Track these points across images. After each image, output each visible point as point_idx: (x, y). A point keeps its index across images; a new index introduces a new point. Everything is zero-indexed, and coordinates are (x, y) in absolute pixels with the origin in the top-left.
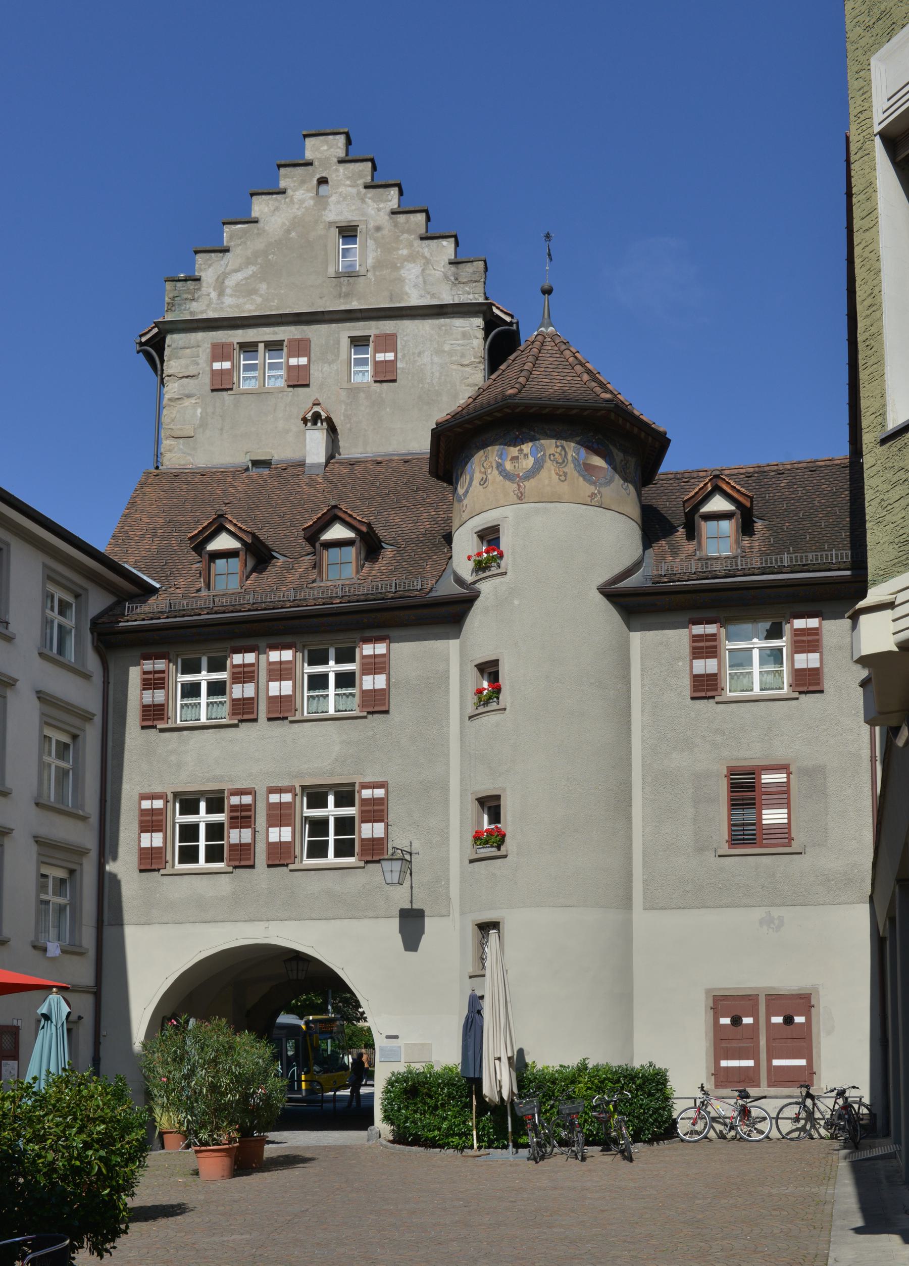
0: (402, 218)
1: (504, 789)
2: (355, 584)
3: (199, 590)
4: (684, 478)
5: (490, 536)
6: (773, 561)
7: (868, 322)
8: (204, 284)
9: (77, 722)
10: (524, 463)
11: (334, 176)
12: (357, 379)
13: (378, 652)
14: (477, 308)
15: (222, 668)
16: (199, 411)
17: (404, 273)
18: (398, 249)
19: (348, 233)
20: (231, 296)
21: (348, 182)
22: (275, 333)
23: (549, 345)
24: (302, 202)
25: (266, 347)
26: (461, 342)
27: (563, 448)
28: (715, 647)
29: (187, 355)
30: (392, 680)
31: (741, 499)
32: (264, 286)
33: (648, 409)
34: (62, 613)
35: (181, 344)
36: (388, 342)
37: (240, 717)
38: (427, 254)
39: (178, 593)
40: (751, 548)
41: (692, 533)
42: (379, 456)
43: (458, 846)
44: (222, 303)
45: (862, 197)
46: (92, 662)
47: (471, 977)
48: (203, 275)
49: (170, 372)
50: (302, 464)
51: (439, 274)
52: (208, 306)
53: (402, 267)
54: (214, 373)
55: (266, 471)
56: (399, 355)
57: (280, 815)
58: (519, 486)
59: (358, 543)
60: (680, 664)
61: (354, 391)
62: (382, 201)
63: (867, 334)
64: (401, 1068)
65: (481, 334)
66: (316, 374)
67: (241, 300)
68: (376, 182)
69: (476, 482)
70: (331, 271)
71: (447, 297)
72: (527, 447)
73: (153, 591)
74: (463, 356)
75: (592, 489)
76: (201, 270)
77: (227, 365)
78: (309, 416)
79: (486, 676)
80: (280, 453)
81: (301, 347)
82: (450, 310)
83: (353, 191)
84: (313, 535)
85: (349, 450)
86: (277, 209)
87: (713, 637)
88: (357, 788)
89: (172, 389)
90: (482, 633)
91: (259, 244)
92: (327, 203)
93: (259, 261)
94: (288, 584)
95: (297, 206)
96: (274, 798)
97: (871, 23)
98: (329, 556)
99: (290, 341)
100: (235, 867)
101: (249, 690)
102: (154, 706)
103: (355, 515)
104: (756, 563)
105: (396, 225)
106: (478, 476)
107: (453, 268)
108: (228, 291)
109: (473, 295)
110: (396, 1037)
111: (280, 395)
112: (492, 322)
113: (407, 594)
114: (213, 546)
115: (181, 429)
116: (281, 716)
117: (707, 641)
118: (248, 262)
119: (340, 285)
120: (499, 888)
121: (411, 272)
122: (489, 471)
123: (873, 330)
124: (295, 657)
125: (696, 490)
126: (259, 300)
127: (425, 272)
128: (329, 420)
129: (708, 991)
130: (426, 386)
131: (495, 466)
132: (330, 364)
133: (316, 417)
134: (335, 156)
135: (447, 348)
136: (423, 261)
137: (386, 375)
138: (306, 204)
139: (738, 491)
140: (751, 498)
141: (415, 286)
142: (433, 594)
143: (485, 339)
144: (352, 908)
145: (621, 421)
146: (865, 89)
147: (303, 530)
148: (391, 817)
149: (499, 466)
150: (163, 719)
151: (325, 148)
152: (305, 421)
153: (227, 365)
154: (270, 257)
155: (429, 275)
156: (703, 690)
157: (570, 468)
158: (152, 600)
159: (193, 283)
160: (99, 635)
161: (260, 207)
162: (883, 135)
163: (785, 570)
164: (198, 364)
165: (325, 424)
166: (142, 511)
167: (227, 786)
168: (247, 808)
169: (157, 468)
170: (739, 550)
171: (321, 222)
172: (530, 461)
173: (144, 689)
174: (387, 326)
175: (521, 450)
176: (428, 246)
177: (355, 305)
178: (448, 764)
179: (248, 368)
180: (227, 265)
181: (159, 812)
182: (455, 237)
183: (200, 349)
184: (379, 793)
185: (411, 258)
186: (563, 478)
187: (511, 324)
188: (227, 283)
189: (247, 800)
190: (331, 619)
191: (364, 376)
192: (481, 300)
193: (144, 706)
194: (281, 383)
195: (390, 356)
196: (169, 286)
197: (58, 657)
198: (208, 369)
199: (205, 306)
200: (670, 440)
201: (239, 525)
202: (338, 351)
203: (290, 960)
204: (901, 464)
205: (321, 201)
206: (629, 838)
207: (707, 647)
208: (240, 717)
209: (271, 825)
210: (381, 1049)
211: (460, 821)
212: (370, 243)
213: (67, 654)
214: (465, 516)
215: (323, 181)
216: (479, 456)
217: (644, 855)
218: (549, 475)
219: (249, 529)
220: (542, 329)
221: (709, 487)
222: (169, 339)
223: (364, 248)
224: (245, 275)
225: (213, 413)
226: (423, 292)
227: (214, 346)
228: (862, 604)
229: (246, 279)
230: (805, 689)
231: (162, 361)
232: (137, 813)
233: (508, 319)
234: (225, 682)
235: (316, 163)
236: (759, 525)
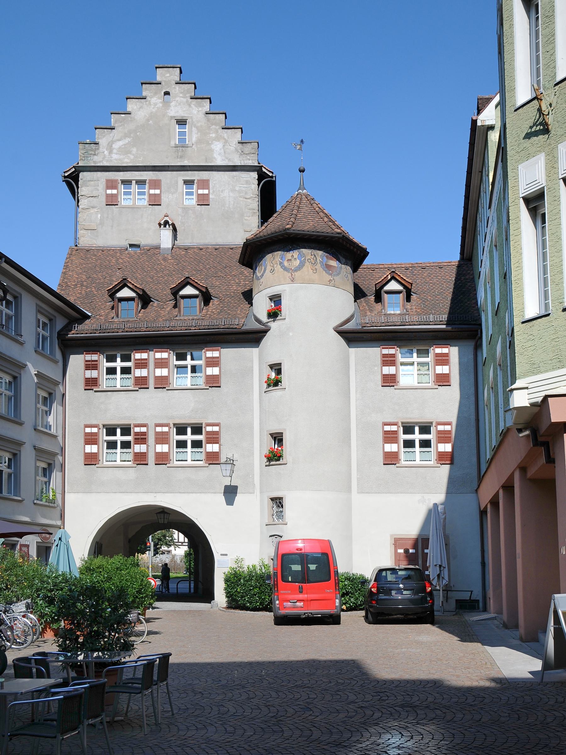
0: (212, 116)
1: (285, 430)
2: (196, 317)
3: (113, 318)
4: (373, 269)
5: (276, 299)
6: (424, 318)
7: (517, 273)
8: (101, 147)
9: (52, 386)
10: (295, 263)
11: (173, 91)
12: (186, 203)
13: (214, 355)
14: (254, 168)
15: (129, 360)
16: (99, 216)
17: (213, 147)
18: (210, 134)
19: (182, 122)
20: (116, 154)
21: (181, 95)
22: (141, 176)
23: (304, 200)
24: (155, 104)
25: (136, 182)
26: (245, 186)
27: (315, 256)
28: (394, 361)
29: (90, 184)
30: (222, 370)
31: (406, 284)
32: (134, 150)
33: (358, 237)
34: (43, 329)
35: (88, 178)
36: (204, 184)
37: (140, 386)
38: (226, 137)
39: (101, 319)
40: (411, 309)
41: (378, 298)
42: (202, 245)
43: (258, 459)
44: (112, 157)
45: (514, 221)
46: (58, 355)
47: (266, 525)
48: (100, 141)
49: (83, 194)
50: (158, 247)
51: (232, 148)
52: (103, 158)
53: (212, 143)
54: (107, 195)
55: (138, 250)
56: (211, 191)
57: (162, 438)
58: (292, 275)
59: (200, 297)
60: (376, 368)
61: (186, 209)
62: (200, 106)
63: (516, 278)
64: (227, 570)
65: (257, 182)
66: (164, 199)
67: (122, 157)
68: (197, 96)
69: (268, 271)
70: (172, 143)
71: (237, 161)
72: (295, 253)
73: (88, 317)
74: (246, 193)
75: (330, 277)
76: (99, 138)
77: (115, 192)
78: (162, 222)
79: (274, 370)
80: (145, 240)
81: (156, 184)
82: (239, 168)
83: (185, 100)
84: (175, 292)
85: (183, 240)
86: (141, 107)
87: (393, 356)
88: (204, 426)
89: (83, 203)
90: (272, 348)
91: (132, 126)
92: (169, 106)
93: (132, 135)
94: (161, 317)
95: (153, 107)
96: (159, 429)
97: (519, 151)
98: (182, 302)
99: (150, 180)
100: (138, 464)
101: (143, 373)
102: (92, 378)
103: (199, 282)
104: (415, 318)
105: (208, 120)
106: (269, 268)
107: (240, 145)
108: (115, 151)
109: (252, 162)
110: (226, 555)
111: (145, 209)
112: (262, 176)
113: (231, 327)
114: (120, 295)
115: (89, 225)
116: (162, 386)
117: (390, 357)
118: (126, 136)
119: (178, 151)
120: (280, 480)
121: (217, 146)
122: (275, 266)
123: (519, 277)
124: (169, 356)
125: (383, 278)
126: (132, 157)
127: (224, 147)
128: (173, 225)
129: (391, 536)
130: (226, 208)
131: (278, 263)
132: (172, 194)
133: (166, 223)
134: (174, 80)
135: (237, 188)
136: (223, 141)
137: (203, 201)
138: (158, 106)
139: (405, 280)
140: (412, 284)
141: (220, 154)
142: (244, 328)
143: (259, 185)
144: (202, 488)
145: (348, 245)
146: (516, 177)
147: (171, 289)
148: (222, 441)
149: (281, 263)
150: (97, 386)
151: (168, 75)
152: (160, 225)
153: (115, 192)
154: (138, 134)
155: (227, 148)
156: (388, 382)
157: (318, 266)
158: (87, 322)
159: (95, 145)
160: (62, 340)
161: (132, 105)
162: (523, 198)
163: (431, 323)
164: (98, 190)
165: (171, 226)
166: (73, 271)
167: (132, 422)
168: (144, 434)
169: (76, 246)
170: (405, 310)
171: (166, 117)
172: (297, 262)
173: (86, 370)
174: (204, 175)
175: (292, 256)
176: (227, 133)
177: (186, 163)
178: (253, 415)
179: (125, 193)
180: (114, 137)
181: (96, 434)
182: (241, 129)
183: (99, 182)
184: (216, 429)
185: (218, 139)
186: (315, 271)
187: (272, 177)
188: (114, 146)
189: (144, 429)
190: (189, 338)
191: (192, 201)
192: (256, 164)
193: (86, 379)
194: (146, 203)
195: (206, 192)
196: (81, 146)
197: (42, 352)
198: (104, 193)
199: (102, 158)
200: (368, 253)
201: (135, 284)
202: (177, 187)
203: (159, 513)
204: (531, 333)
205: (166, 104)
206: (350, 456)
207: (390, 361)
208: (140, 386)
209: (157, 443)
210: (218, 561)
211: (261, 446)
212: (194, 129)
213: (46, 350)
214: (261, 288)
215: (167, 93)
216: (269, 257)
217: (358, 465)
218: (307, 269)
219: (141, 287)
220: (300, 191)
221: (389, 277)
222: (82, 175)
223: (191, 131)
224: (124, 143)
225: (107, 217)
226: (224, 158)
227: (107, 181)
228: (514, 386)
229: (125, 145)
230: (442, 384)
231: (78, 187)
232: (83, 434)
233: (271, 175)
234: (130, 368)
235: (163, 83)
236: (414, 297)
